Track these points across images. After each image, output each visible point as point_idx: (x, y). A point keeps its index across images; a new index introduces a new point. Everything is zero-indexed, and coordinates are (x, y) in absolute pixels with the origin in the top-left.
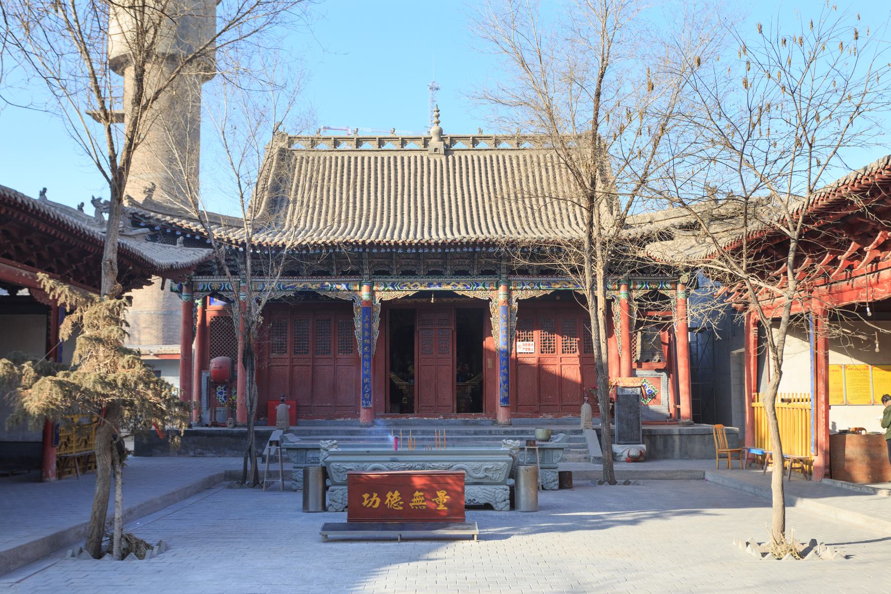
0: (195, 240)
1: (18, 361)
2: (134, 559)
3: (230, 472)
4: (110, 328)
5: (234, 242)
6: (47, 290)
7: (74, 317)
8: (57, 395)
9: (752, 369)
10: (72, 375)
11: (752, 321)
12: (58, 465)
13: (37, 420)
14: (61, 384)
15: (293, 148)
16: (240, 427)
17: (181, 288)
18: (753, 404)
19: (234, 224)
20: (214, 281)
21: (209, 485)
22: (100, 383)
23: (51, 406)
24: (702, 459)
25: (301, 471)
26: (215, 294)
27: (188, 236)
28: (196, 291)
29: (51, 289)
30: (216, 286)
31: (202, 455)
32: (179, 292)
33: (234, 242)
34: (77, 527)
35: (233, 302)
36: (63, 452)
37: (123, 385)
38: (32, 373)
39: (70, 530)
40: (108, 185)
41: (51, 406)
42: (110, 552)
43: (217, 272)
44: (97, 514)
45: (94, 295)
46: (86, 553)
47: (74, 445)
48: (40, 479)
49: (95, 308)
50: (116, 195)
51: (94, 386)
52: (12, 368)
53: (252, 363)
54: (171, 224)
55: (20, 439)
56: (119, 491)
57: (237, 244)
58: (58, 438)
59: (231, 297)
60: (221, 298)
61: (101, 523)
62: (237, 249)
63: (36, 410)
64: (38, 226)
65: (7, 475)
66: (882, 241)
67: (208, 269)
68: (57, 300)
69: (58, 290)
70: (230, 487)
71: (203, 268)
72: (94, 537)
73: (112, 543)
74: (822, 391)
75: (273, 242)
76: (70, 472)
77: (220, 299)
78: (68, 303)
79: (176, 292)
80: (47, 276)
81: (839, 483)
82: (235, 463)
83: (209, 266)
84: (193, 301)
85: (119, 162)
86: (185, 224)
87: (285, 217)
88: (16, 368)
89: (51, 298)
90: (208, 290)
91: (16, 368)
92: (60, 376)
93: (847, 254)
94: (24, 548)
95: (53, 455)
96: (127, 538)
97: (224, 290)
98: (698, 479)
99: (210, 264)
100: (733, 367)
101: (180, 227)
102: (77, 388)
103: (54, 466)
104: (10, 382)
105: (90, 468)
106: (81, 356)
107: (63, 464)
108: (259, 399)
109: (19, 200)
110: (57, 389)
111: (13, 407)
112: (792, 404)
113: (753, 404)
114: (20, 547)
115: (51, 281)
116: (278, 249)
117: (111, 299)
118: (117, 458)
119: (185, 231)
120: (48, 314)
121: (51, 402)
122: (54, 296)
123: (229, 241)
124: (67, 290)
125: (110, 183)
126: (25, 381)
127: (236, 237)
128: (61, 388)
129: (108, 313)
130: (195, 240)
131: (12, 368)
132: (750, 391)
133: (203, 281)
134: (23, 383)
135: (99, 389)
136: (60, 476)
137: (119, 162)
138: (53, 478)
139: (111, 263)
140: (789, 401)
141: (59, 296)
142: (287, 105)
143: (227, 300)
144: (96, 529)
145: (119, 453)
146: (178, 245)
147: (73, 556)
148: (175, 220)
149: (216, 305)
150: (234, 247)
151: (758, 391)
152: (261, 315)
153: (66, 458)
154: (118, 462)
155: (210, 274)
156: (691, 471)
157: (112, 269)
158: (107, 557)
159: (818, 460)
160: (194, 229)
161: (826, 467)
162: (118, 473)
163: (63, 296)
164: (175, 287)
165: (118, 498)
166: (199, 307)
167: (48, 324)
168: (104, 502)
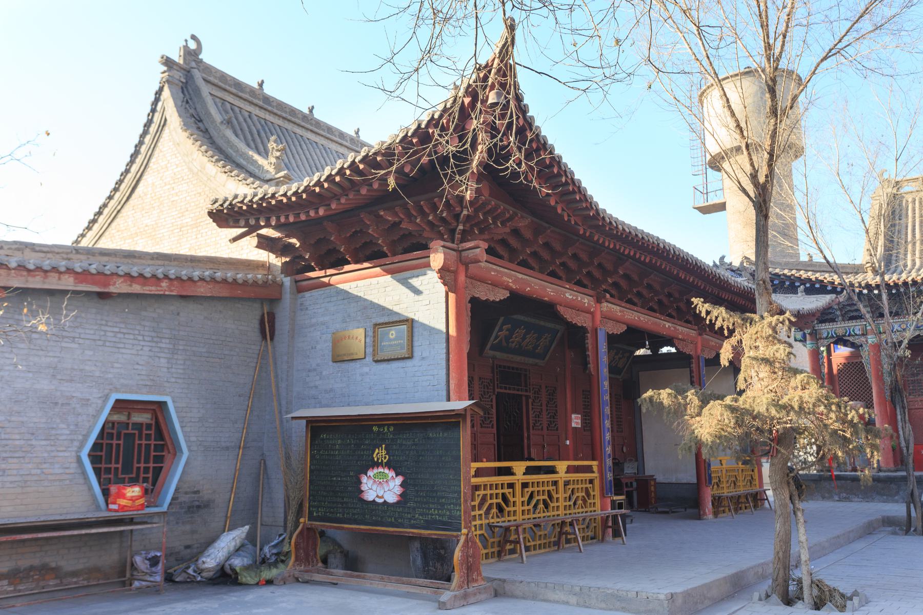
0: (814, 288)
1: (681, 392)
2: (833, 610)
3: (888, 517)
4: (775, 348)
5: (857, 285)
6: (703, 314)
7: (733, 340)
8: (729, 419)
10: (741, 399)
12: (713, 504)
13: (711, 447)
14: (732, 409)
15: (902, 191)
16: (885, 471)
17: (804, 336)
19: (857, 270)
20: (839, 327)
21: (869, 530)
22: (775, 406)
23: (723, 433)
26: (841, 340)
27: (808, 285)
28: (821, 338)
29: (708, 313)
30: (840, 332)
31: (847, 499)
32: (803, 340)
33: (857, 285)
34: (755, 566)
35: (861, 346)
36: (716, 492)
37: (800, 408)
38: (696, 402)
39: (748, 569)
40: (751, 204)
41: (723, 433)
42: (800, 598)
43: (840, 318)
44: (781, 554)
45: (753, 315)
46: (775, 598)
47: (724, 485)
48: (699, 517)
49: (757, 327)
50: (762, 211)
51: (767, 410)
52: (676, 397)
53: (903, 401)
54: (789, 277)
55: (674, 481)
56: (802, 530)
57: (860, 286)
58: (710, 478)
59: (857, 341)
60: (845, 343)
61: (786, 561)
62: (861, 292)
63: (708, 436)
64: (678, 274)
65: (667, 513)
67: (831, 316)
68: (715, 324)
69: (715, 313)
70: (895, 533)
71: (825, 315)
72: (780, 580)
73: (801, 588)
75: (902, 280)
76: (724, 512)
77: (845, 345)
78: (725, 327)
79: (800, 341)
80: (702, 300)
82: (897, 509)
83: (831, 313)
84: (818, 348)
85: (762, 179)
86: (803, 274)
87: (906, 255)
88: (680, 397)
89: (708, 322)
90: (832, 337)
91: (680, 397)
92: (728, 400)
94: (708, 586)
95: (708, 494)
96: (818, 584)
97: (849, 335)
99: (835, 308)
101: (799, 278)
102: (749, 412)
103: (710, 505)
104: (676, 412)
105: (741, 509)
106: (746, 381)
107: (717, 501)
108: (915, 438)
109: (661, 245)
110: (727, 414)
111: (683, 436)
114: (705, 585)
115: (707, 305)
116: (905, 283)
117: (772, 316)
118: (795, 493)
119: (803, 282)
120: (690, 363)
121: (722, 429)
122: (711, 321)
123: (852, 285)
124: (724, 311)
125: (753, 201)
126: (691, 410)
127: (859, 280)
128: (732, 412)
129: (771, 332)
130: (814, 288)
131: (676, 397)
133: (826, 329)
134: (689, 412)
135: (773, 412)
136: (716, 514)
137: (762, 179)
138: (711, 516)
139: (764, 282)
141: (717, 318)
142: (909, 129)
143: (853, 345)
144: (781, 572)
145: (797, 488)
146: (800, 294)
147: (760, 599)
148: (794, 272)
149: (841, 353)
150: (857, 290)
152: (908, 348)
153: (719, 497)
154: (797, 497)
155: (833, 320)
157: (766, 289)
158: (799, 605)
160: (813, 278)
162: (798, 509)
163: (720, 319)
164: (799, 335)
165: (803, 538)
166: (825, 354)
167: (691, 372)
168: (786, 542)
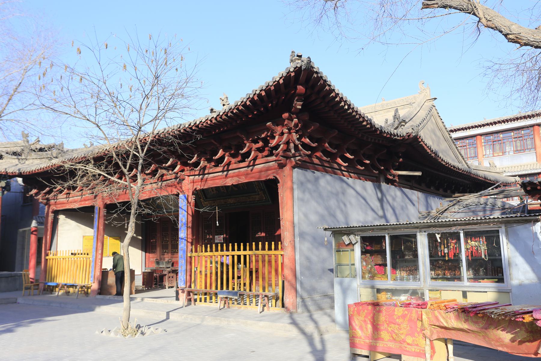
9: (48, 237)
11: (50, 210)
18: (47, 257)
24: (5, 292)
25: (230, 257)
66: (154, 169)
74: (100, 248)
81: (108, 297)
93: (44, 192)
98: (12, 303)
100: (19, 239)
112: (77, 255)
113: (47, 257)
132: (46, 250)
140: (75, 254)
151: (50, 250)
156: (8, 299)
159: (95, 286)
161: (99, 289)
